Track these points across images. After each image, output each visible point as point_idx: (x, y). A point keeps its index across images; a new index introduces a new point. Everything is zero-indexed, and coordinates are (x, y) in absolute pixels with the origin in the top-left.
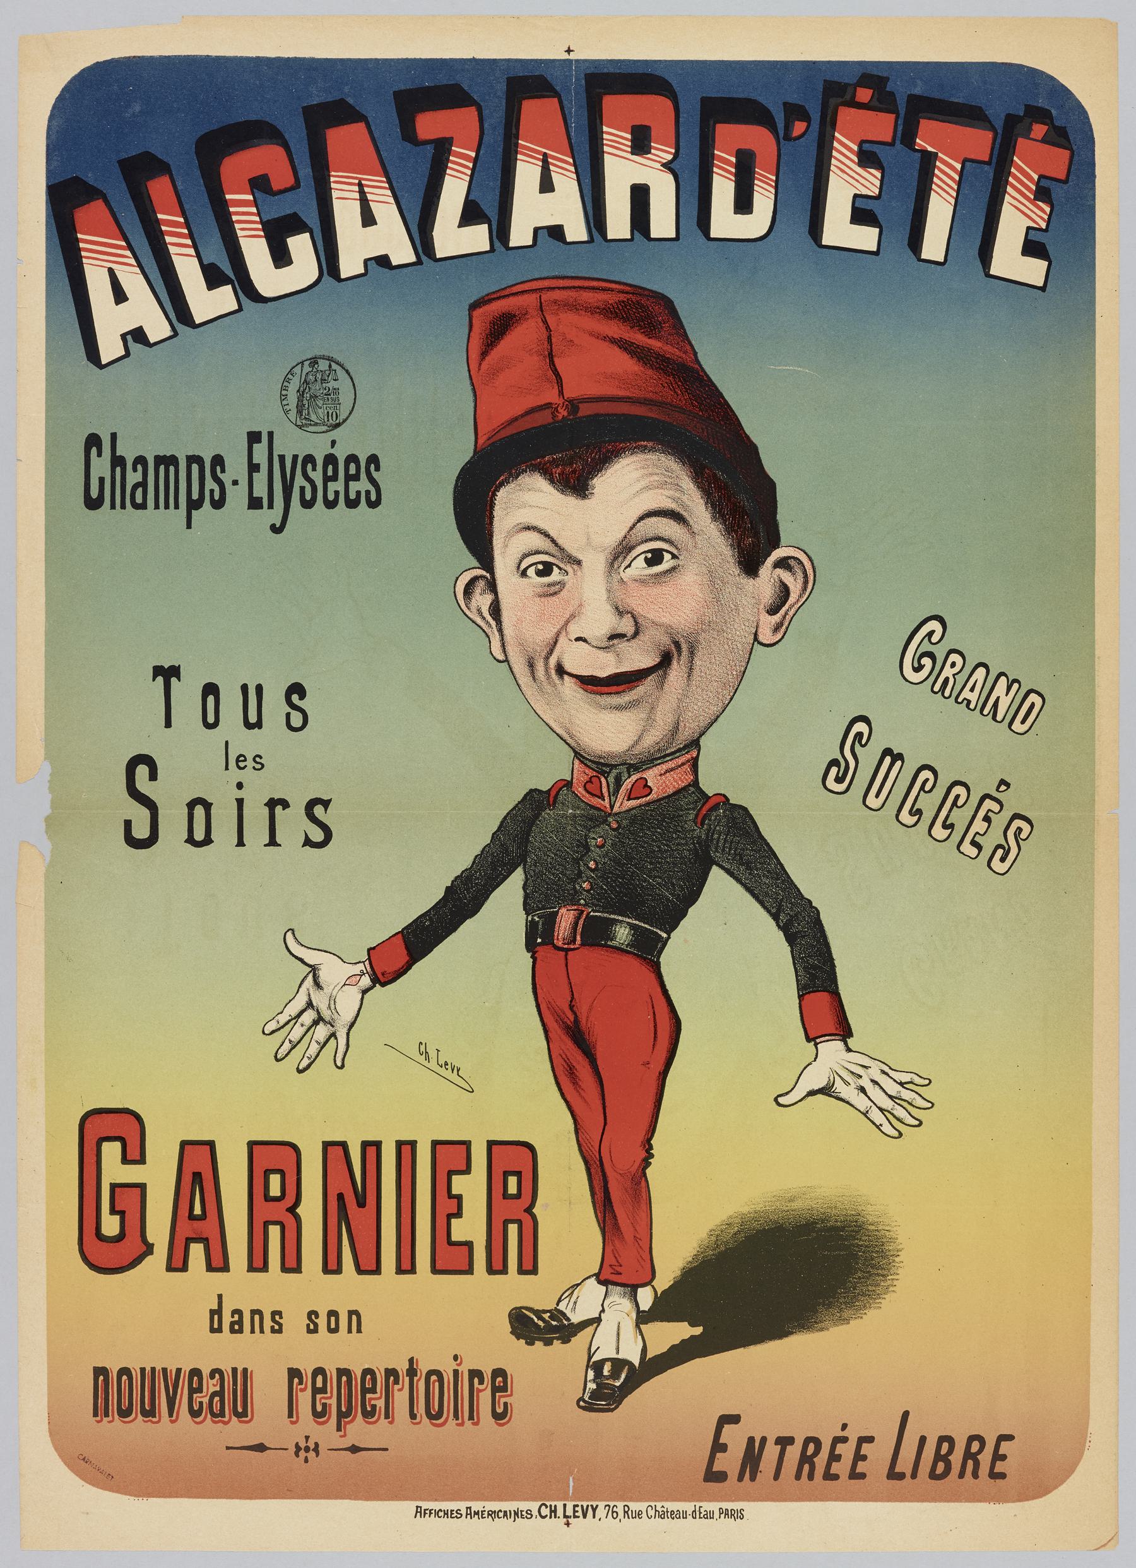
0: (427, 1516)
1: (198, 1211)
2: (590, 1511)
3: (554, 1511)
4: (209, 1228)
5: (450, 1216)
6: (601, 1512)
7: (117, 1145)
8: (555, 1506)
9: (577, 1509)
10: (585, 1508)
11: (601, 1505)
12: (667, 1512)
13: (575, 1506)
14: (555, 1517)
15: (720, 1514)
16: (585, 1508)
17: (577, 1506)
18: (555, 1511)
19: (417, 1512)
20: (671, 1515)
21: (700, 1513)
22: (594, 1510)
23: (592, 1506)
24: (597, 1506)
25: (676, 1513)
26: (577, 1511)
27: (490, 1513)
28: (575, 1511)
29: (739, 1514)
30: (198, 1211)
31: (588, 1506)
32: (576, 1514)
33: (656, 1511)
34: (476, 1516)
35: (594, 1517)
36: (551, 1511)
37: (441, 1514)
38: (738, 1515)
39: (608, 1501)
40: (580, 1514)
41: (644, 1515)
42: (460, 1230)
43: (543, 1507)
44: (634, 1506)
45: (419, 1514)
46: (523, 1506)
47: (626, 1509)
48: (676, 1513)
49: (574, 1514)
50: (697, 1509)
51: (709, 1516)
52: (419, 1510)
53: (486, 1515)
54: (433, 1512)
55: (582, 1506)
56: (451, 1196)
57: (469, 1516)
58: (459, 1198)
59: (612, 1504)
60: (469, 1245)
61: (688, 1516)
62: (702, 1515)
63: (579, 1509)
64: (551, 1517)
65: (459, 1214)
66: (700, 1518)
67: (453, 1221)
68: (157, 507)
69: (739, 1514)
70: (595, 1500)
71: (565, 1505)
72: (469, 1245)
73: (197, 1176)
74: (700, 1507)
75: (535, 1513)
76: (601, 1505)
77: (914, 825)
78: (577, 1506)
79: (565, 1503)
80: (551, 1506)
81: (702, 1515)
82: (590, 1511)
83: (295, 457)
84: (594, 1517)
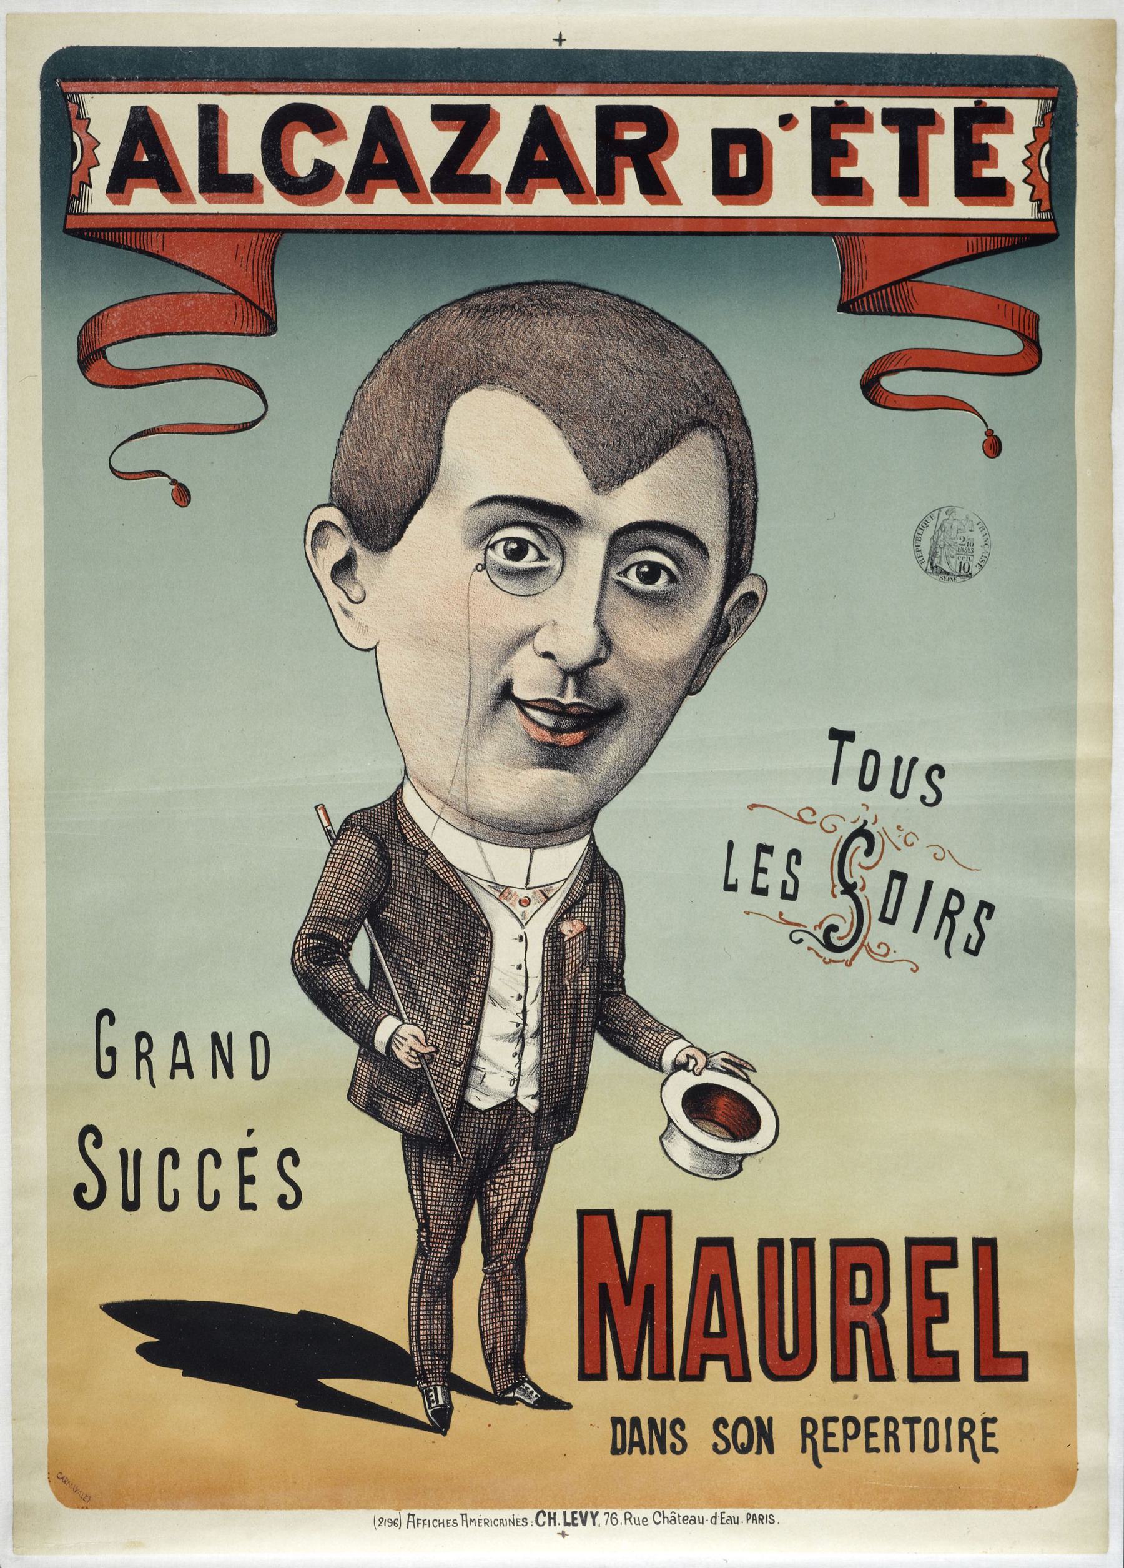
0: (421, 1526)
1: (715, 1327)
2: (589, 1517)
3: (552, 1518)
4: (730, 1345)
5: (931, 1321)
6: (601, 1518)
7: (935, 1272)
8: (555, 1514)
9: (576, 1516)
10: (584, 1514)
11: (602, 1511)
12: (679, 1516)
13: (574, 1513)
14: (555, 1525)
15: (748, 1520)
16: (584, 1514)
17: (576, 1512)
18: (554, 1519)
19: (408, 1521)
20: (683, 1520)
21: (722, 1518)
22: (594, 1517)
23: (592, 1513)
24: (597, 1513)
25: (689, 1519)
26: (576, 1519)
27: (486, 1521)
28: (574, 1519)
29: (768, 1519)
30: (715, 1327)
31: (587, 1513)
32: (576, 1522)
33: (664, 1518)
34: (473, 1524)
35: (594, 1524)
36: (550, 1518)
37: (436, 1523)
38: (771, 1519)
39: (659, 1508)
40: (579, 1521)
41: (650, 1521)
42: (943, 1337)
43: (541, 1514)
44: (638, 1513)
45: (465, 1522)
46: (520, 1514)
47: (628, 1516)
48: (689, 1519)
49: (573, 1521)
50: (719, 1514)
51: (734, 1520)
52: (411, 1519)
53: (483, 1524)
54: (426, 1522)
55: (581, 1512)
56: (930, 1295)
57: (411, 1524)
58: (943, 1297)
59: (611, 1511)
60: (954, 1355)
61: (705, 1520)
62: (724, 1521)
63: (577, 1516)
64: (550, 1524)
65: (944, 1318)
66: (722, 1523)
67: (936, 1328)
68: (949, 1449)
69: (768, 1519)
70: (596, 1507)
71: (565, 1513)
72: (954, 1355)
73: (715, 1283)
74: (722, 1513)
75: (531, 1518)
76: (602, 1511)
77: (827, 832)
78: (576, 1512)
79: (463, 1511)
80: (549, 1513)
81: (724, 1521)
82: (589, 1517)
83: (948, 1421)
84: (594, 1524)
